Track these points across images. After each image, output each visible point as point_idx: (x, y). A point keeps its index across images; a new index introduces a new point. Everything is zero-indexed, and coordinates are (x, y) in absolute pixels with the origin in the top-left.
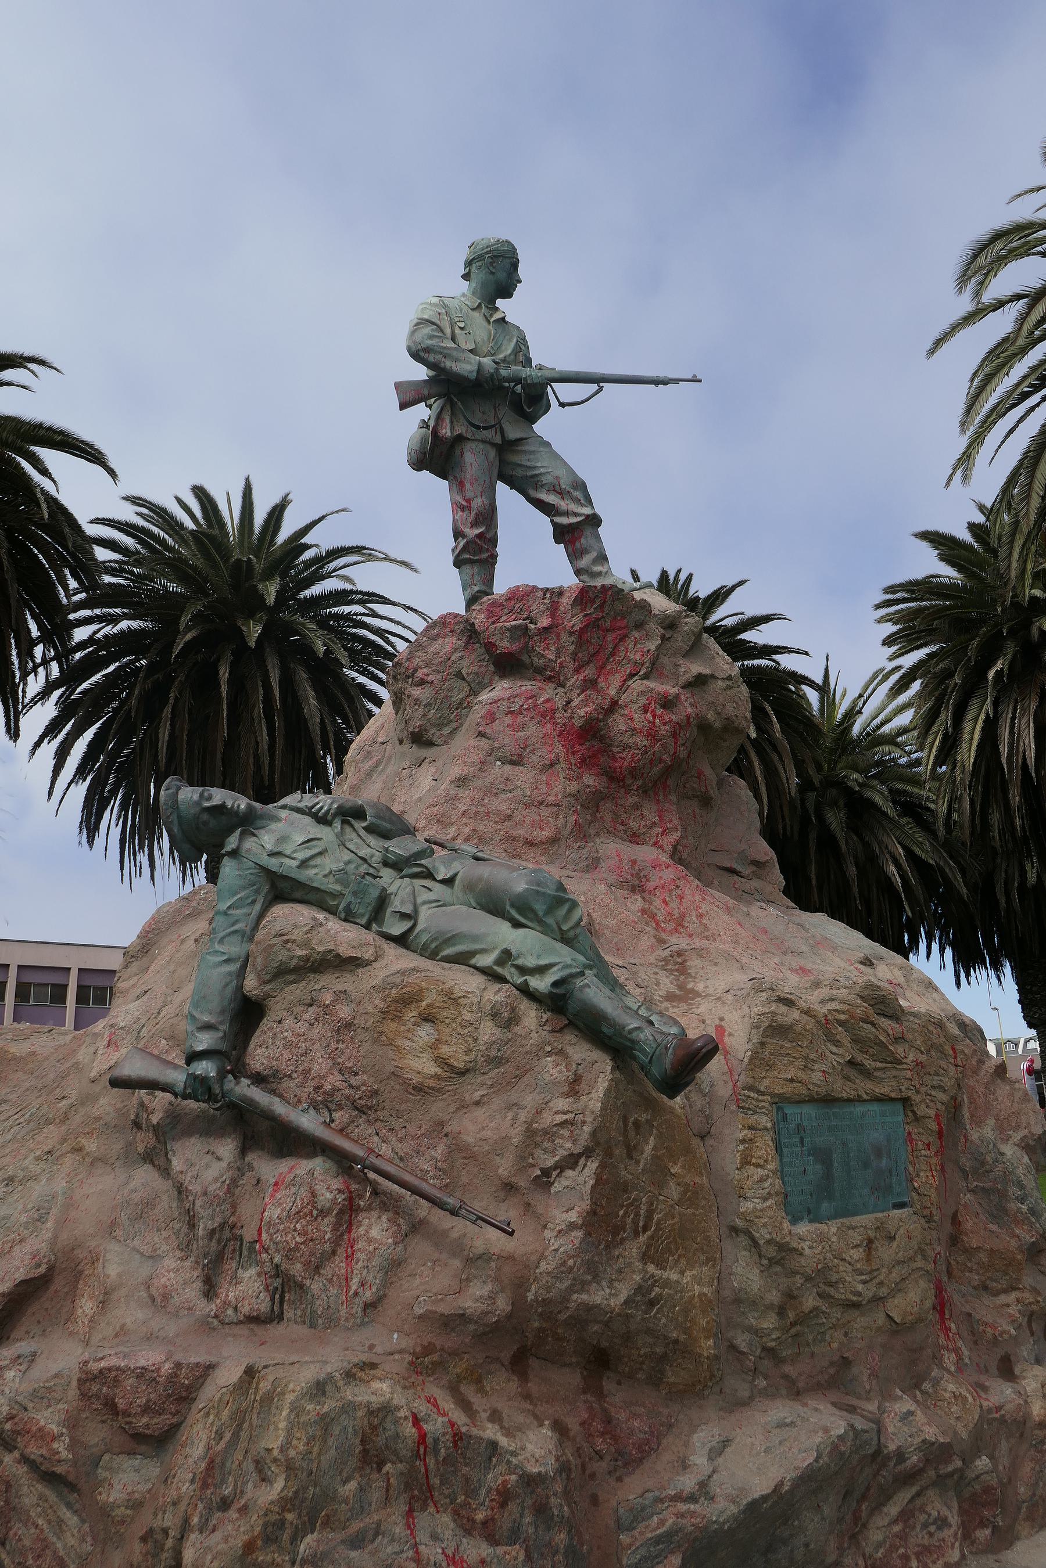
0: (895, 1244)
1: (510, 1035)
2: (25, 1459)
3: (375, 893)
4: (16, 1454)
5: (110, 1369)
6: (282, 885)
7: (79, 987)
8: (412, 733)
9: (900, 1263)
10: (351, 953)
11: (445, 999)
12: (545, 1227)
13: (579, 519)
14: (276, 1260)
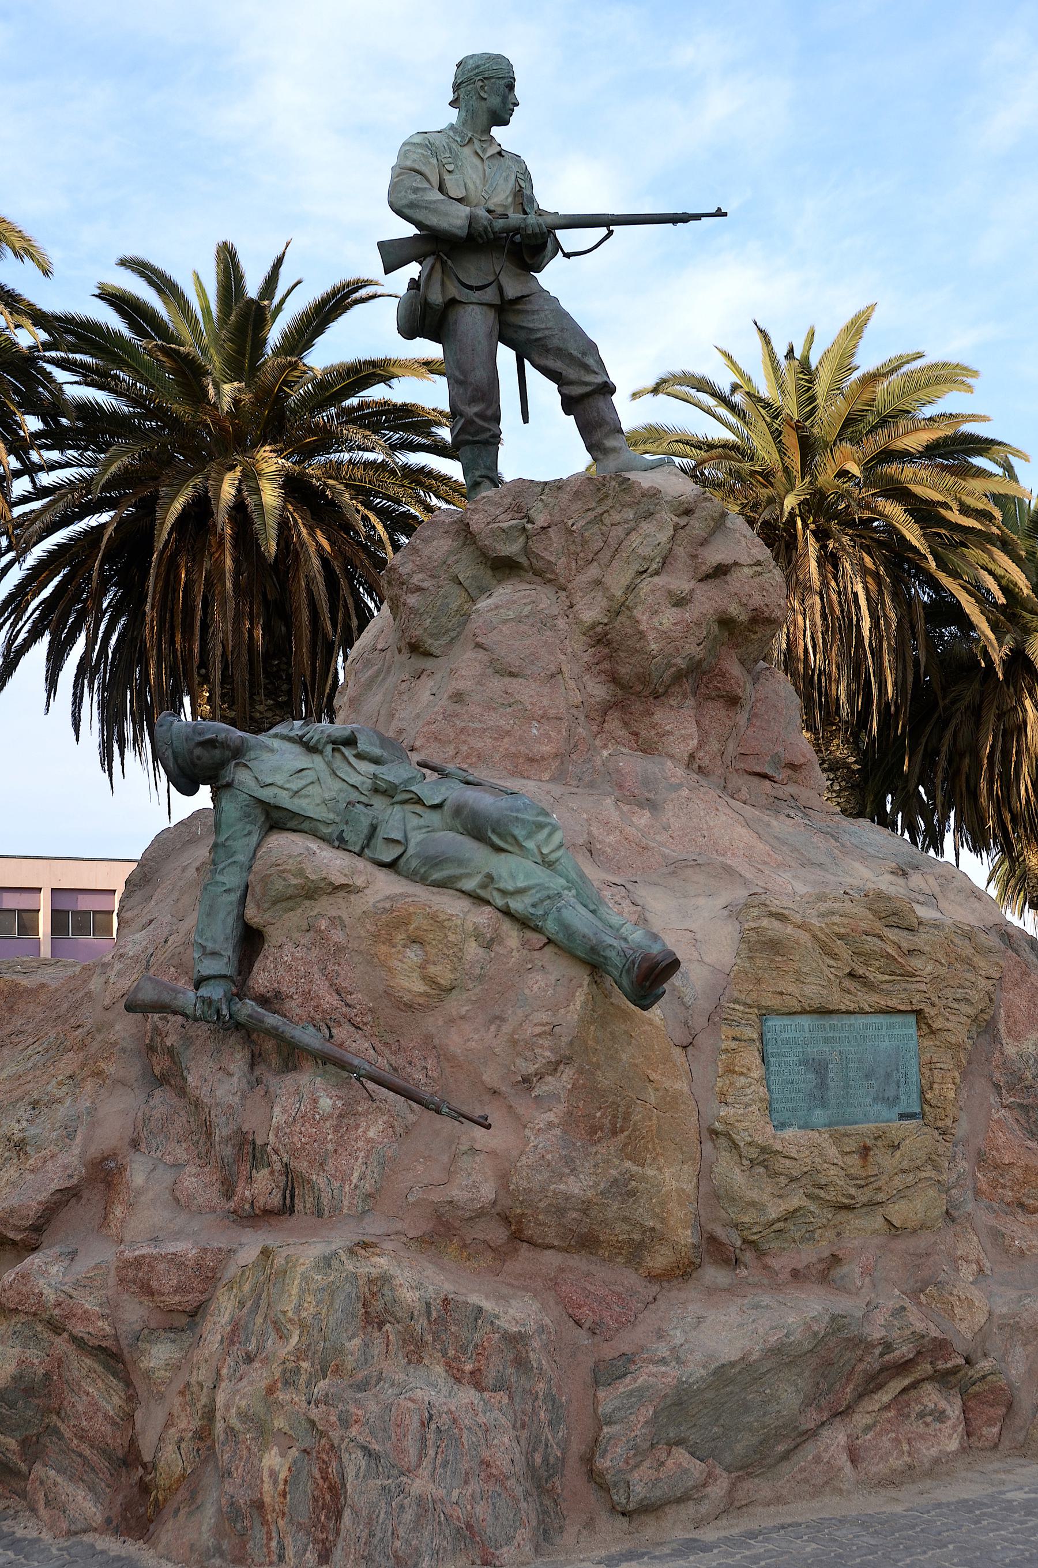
0: (898, 1154)
1: (493, 954)
2: (75, 1339)
3: (365, 823)
4: (65, 1335)
5: (143, 1256)
6: (275, 815)
7: (54, 912)
8: (409, 644)
9: (903, 1171)
10: (343, 880)
11: (431, 921)
12: (525, 1127)
13: (588, 389)
14: (285, 1160)
